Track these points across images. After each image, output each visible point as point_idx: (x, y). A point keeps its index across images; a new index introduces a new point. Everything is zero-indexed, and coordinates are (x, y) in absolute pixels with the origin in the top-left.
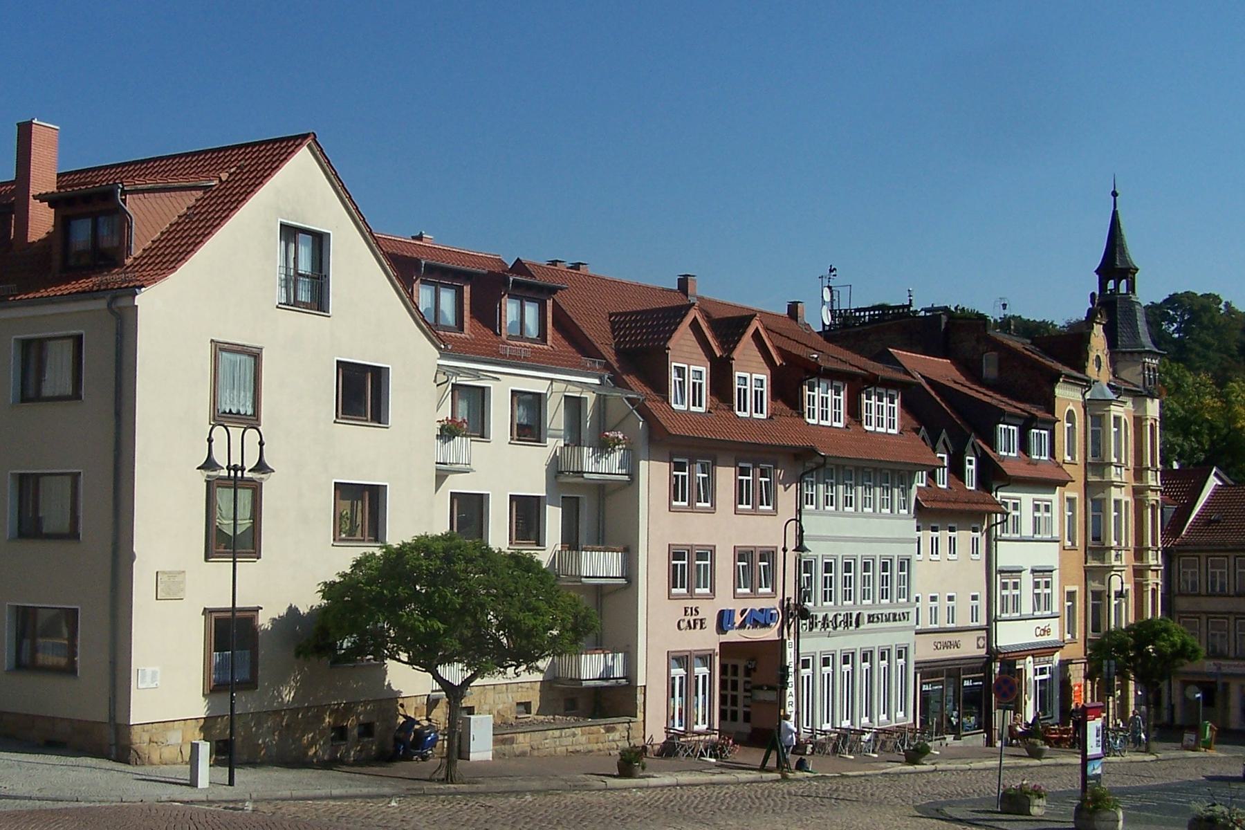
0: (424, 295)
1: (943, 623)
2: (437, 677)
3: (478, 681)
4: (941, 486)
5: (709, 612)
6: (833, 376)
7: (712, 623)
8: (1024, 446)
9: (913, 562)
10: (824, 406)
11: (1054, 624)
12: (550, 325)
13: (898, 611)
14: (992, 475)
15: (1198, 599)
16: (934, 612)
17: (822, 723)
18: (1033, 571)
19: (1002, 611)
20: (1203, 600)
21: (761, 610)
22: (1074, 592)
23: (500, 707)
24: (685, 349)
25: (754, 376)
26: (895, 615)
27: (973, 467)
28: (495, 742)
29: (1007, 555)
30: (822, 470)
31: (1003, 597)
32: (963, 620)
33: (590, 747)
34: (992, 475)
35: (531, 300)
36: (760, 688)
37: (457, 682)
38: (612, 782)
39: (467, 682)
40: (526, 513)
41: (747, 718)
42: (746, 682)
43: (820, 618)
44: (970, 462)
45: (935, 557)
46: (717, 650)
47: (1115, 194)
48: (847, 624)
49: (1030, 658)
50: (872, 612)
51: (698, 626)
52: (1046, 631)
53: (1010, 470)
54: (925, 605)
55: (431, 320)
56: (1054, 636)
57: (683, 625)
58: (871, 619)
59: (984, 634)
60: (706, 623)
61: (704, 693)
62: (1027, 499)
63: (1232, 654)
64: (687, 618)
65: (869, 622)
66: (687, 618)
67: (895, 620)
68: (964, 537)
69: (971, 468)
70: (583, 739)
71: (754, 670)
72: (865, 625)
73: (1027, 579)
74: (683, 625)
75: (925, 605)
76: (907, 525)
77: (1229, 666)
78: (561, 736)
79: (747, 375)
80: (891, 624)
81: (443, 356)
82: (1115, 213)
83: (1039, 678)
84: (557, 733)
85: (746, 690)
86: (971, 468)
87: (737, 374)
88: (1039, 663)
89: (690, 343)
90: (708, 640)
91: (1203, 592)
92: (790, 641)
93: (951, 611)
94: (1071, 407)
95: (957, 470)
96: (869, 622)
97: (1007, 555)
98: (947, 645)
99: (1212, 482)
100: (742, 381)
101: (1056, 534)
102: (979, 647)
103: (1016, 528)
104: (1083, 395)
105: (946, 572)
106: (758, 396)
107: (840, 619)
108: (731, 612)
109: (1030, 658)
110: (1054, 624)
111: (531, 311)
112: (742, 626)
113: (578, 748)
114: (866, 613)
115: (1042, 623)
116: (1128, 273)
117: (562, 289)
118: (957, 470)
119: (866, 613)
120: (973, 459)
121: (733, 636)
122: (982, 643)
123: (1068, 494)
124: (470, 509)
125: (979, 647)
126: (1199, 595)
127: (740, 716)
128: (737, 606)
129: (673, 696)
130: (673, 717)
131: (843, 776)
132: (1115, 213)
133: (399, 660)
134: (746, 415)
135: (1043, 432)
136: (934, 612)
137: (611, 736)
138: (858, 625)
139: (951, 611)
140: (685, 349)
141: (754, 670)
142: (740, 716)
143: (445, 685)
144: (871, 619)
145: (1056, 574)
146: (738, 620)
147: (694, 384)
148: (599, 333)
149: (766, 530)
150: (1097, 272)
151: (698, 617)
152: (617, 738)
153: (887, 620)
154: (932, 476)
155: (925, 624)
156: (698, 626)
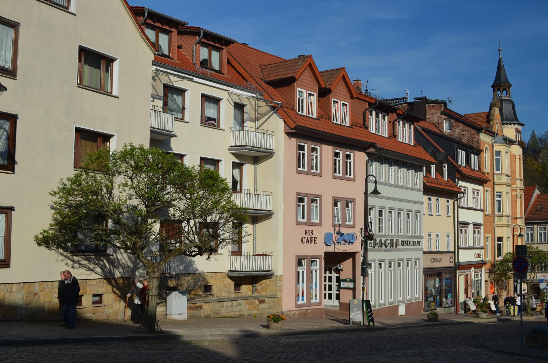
17: (389, 232)
18: (474, 225)
24: (304, 81)
25: (342, 102)
28: (190, 308)
29: (464, 216)
41: (338, 297)
46: (323, 256)
48: (391, 245)
49: (473, 269)
50: (403, 240)
51: (313, 242)
52: (479, 256)
55: (153, 41)
58: (403, 243)
59: (452, 255)
61: (303, 282)
62: (470, 187)
65: (402, 245)
66: (306, 237)
69: (445, 170)
72: (400, 247)
80: (412, 247)
86: (445, 170)
89: (307, 78)
95: (439, 171)
97: (497, 188)
99: (537, 192)
102: (450, 262)
105: (435, 225)
109: (473, 269)
115: (478, 251)
118: (439, 171)
119: (400, 240)
122: (452, 260)
125: (450, 262)
127: (334, 296)
129: (298, 282)
130: (298, 295)
137: (261, 306)
140: (304, 81)
142: (334, 296)
144: (403, 243)
145: (482, 227)
151: (313, 236)
153: (410, 245)
155: (426, 249)
156: (313, 242)
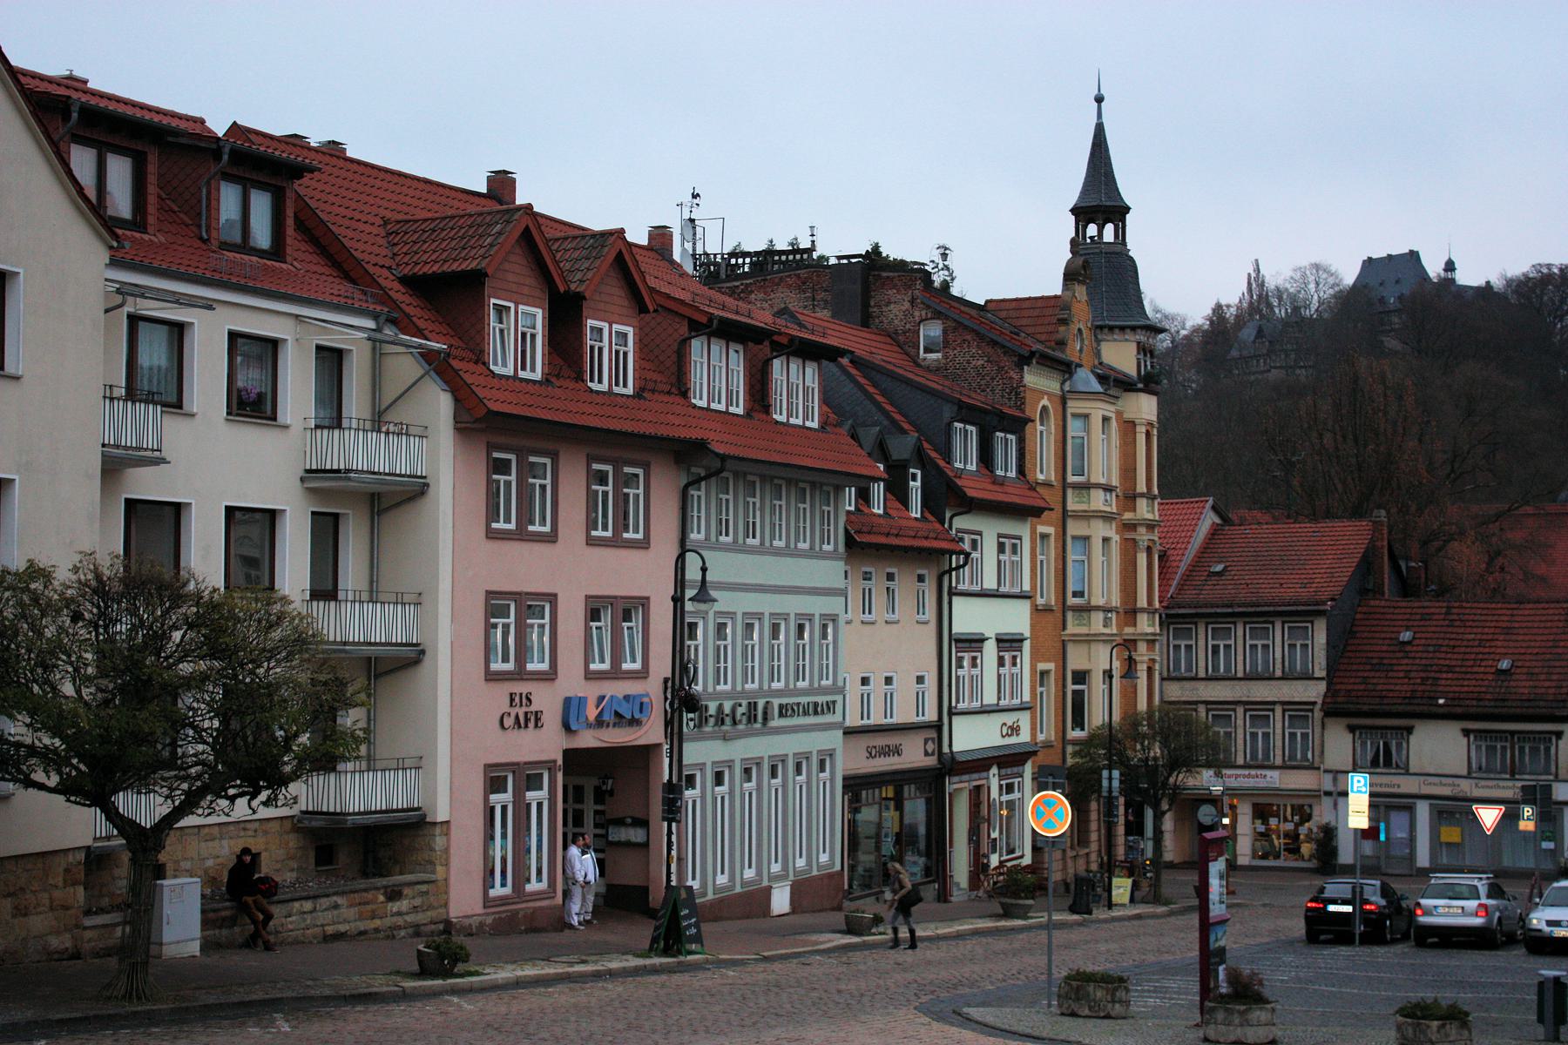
0: (82, 161)
1: (876, 718)
2: (112, 815)
3: (189, 821)
4: (876, 511)
5: (547, 700)
6: (730, 332)
7: (552, 719)
8: (986, 458)
9: (841, 622)
10: (716, 377)
11: (1024, 720)
12: (290, 222)
13: (821, 699)
14: (947, 496)
15: (1193, 683)
16: (865, 700)
18: (999, 641)
19: (958, 701)
20: (1201, 685)
21: (626, 698)
22: (1048, 672)
23: (210, 863)
26: (816, 704)
27: (918, 483)
29: (968, 617)
30: (713, 480)
31: (958, 678)
32: (904, 714)
33: (362, 926)
34: (947, 496)
35: (120, 151)
36: (620, 822)
37: (146, 822)
38: (410, 984)
39: (168, 821)
40: (251, 529)
42: (596, 812)
43: (712, 710)
44: (914, 479)
45: (867, 617)
46: (560, 762)
47: (1099, 100)
50: (784, 701)
51: (531, 724)
53: (975, 489)
54: (854, 690)
56: (1025, 737)
57: (509, 722)
58: (784, 711)
60: (544, 718)
62: (990, 530)
63: (1240, 761)
64: (513, 711)
65: (781, 715)
66: (513, 711)
67: (816, 713)
68: (905, 585)
70: (351, 913)
71: (611, 793)
72: (776, 722)
73: (990, 649)
74: (509, 722)
75: (854, 690)
76: (831, 572)
77: (1237, 776)
78: (314, 910)
79: (605, 326)
81: (114, 263)
82: (1100, 132)
83: (1005, 798)
84: (308, 905)
85: (596, 826)
87: (590, 322)
88: (1007, 777)
90: (546, 744)
91: (1202, 674)
92: (1382, 826)
93: (889, 699)
94: (1045, 402)
95: (897, 490)
96: (781, 715)
98: (886, 751)
100: (595, 336)
101: (1027, 587)
103: (977, 576)
104: (1062, 384)
106: (619, 359)
107: (740, 710)
108: (582, 701)
109: (994, 770)
110: (1024, 720)
111: (261, 204)
112: (600, 723)
113: (342, 928)
114: (776, 702)
115: (1010, 718)
116: (1117, 212)
117: (312, 170)
118: (897, 490)
119: (776, 702)
120: (919, 473)
121: (588, 739)
122: (931, 747)
123: (1041, 529)
124: (156, 523)
125: (926, 754)
126: (1195, 679)
128: (591, 691)
129: (492, 838)
131: (766, 959)
132: (1100, 132)
133: (41, 787)
134: (604, 387)
135: (969, 427)
136: (865, 700)
137: (395, 906)
138: (765, 719)
139: (889, 699)
141: (611, 793)
143: (125, 826)
145: (1027, 645)
146: (592, 713)
147: (617, 352)
148: (367, 246)
149: (646, 574)
150: (1072, 211)
151: (533, 708)
152: (404, 909)
153: (806, 713)
154: (864, 496)
155: (853, 720)
